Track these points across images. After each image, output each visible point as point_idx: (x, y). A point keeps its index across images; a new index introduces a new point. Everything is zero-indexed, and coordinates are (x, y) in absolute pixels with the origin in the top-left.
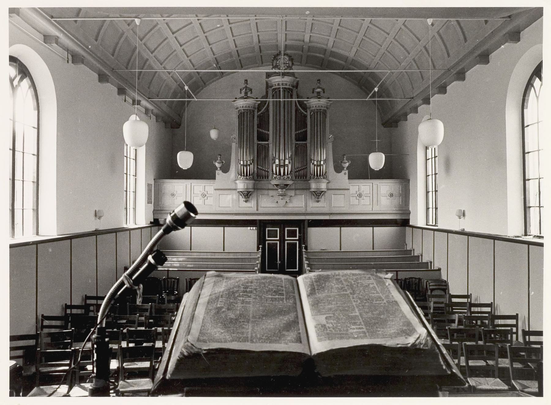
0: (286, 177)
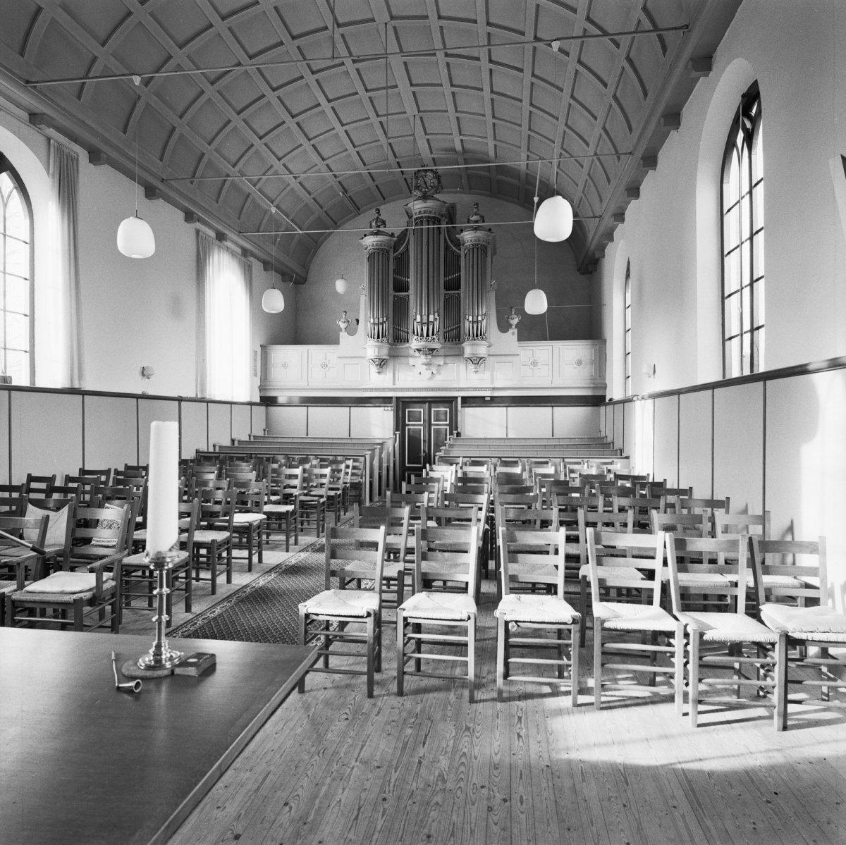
0: (430, 338)
